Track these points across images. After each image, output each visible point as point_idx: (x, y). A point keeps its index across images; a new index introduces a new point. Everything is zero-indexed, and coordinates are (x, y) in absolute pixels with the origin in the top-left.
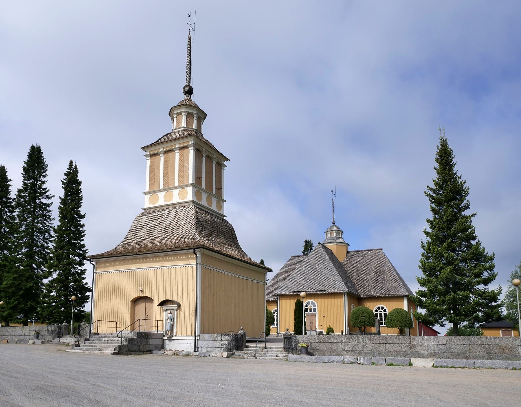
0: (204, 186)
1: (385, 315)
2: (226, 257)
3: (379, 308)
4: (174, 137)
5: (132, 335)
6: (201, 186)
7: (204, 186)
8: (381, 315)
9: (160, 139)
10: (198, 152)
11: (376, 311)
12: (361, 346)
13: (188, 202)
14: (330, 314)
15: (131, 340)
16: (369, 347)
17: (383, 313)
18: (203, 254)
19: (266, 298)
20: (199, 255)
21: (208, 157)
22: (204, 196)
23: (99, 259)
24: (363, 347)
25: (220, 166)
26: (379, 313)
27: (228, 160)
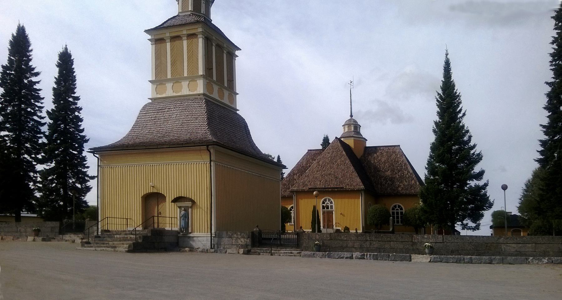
0: (215, 78)
1: (401, 213)
2: (240, 155)
3: (395, 206)
4: (180, 23)
5: (147, 232)
6: (212, 77)
7: (215, 78)
8: (397, 213)
9: (165, 22)
10: (208, 41)
11: (393, 209)
12: (368, 243)
13: (199, 95)
14: (350, 213)
15: (145, 238)
16: (376, 245)
17: (400, 211)
18: (216, 151)
19: (281, 193)
20: (212, 151)
21: (219, 46)
22: (216, 88)
23: (102, 152)
24: (371, 244)
25: (231, 56)
26: (395, 211)
27: (239, 49)
